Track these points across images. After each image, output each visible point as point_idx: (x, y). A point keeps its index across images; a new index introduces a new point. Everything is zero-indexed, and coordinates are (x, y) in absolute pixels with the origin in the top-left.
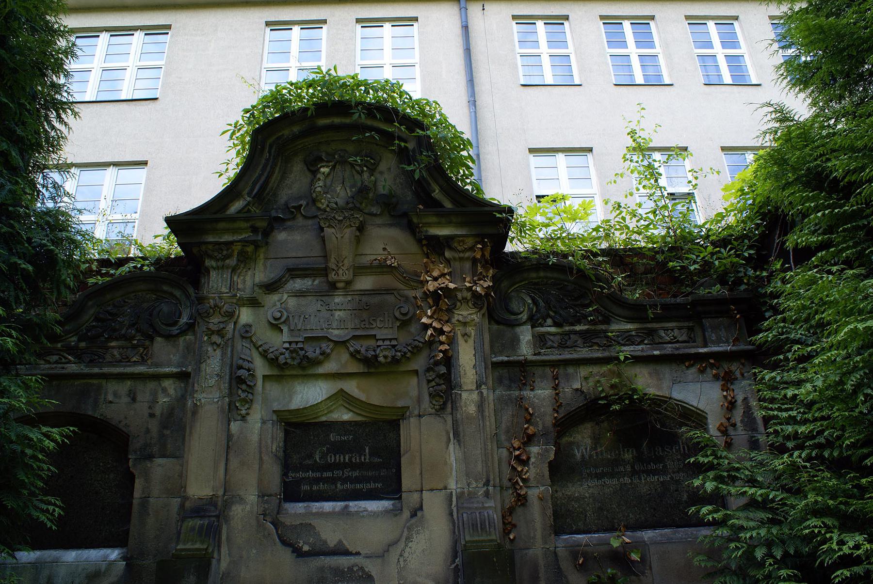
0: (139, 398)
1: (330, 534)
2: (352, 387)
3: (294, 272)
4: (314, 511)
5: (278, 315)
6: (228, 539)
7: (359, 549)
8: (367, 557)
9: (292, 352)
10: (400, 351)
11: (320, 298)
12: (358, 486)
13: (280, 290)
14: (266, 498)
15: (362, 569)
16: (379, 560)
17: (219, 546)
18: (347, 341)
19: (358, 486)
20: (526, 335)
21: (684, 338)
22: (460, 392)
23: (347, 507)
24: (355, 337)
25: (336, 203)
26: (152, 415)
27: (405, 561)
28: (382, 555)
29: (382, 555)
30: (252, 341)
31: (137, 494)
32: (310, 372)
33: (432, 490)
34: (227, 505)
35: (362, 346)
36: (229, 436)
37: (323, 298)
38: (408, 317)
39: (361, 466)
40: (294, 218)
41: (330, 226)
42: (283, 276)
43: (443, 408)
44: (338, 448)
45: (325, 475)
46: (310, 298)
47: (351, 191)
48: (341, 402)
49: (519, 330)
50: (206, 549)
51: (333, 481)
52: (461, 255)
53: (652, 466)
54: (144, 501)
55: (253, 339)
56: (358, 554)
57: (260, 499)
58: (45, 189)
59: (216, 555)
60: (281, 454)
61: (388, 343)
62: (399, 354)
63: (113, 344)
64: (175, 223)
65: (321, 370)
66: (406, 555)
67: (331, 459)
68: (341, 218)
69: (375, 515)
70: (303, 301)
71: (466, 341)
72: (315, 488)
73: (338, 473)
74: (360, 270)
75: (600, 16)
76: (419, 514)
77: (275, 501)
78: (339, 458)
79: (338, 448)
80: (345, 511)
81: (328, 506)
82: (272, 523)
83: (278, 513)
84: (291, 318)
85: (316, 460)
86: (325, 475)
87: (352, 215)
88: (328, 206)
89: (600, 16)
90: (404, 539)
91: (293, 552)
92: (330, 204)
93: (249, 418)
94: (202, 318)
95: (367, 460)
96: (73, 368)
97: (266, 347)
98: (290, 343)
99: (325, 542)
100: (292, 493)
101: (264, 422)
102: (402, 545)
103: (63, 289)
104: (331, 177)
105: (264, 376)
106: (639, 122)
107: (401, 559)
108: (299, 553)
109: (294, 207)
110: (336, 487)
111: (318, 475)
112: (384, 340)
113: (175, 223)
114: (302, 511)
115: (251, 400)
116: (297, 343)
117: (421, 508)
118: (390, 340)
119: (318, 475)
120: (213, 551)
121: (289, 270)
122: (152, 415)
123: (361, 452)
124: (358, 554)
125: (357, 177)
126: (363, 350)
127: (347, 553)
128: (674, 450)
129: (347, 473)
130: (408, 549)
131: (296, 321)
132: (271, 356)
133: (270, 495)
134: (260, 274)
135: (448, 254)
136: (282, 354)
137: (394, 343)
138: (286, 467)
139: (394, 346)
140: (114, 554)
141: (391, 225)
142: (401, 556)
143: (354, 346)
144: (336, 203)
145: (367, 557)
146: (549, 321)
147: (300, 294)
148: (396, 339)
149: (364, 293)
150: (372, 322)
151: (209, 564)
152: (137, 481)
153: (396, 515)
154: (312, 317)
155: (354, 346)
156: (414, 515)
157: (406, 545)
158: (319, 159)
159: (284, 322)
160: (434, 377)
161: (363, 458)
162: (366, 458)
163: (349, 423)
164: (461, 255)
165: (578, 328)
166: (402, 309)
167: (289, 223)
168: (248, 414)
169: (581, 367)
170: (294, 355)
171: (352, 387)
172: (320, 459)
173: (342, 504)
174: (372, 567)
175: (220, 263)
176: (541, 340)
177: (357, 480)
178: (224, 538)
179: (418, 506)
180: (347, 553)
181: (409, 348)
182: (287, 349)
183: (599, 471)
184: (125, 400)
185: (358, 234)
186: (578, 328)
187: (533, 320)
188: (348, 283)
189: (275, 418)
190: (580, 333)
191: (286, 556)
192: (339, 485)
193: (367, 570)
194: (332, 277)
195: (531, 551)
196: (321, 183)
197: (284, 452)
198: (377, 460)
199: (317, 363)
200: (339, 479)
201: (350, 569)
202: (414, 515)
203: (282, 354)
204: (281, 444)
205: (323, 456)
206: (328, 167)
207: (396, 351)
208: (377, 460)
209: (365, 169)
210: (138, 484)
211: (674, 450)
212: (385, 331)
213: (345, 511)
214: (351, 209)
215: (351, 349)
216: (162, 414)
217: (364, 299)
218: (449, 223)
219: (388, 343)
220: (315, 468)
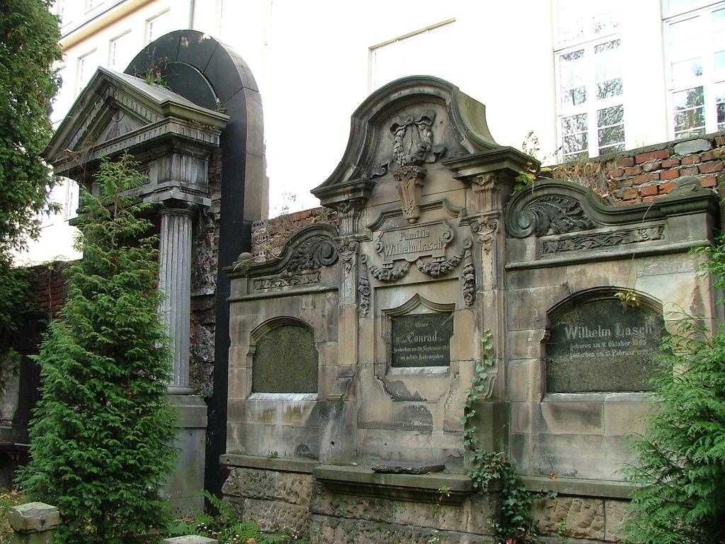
0: (317, 306)
1: (412, 388)
15: (425, 409)
16: (435, 405)
18: (416, 261)
19: (430, 357)
20: (531, 244)
21: (656, 235)
23: (422, 371)
24: (421, 258)
26: (323, 316)
32: (398, 284)
38: (451, 238)
39: (433, 344)
44: (420, 332)
49: (526, 240)
51: (417, 353)
52: (483, 188)
53: (622, 344)
56: (426, 400)
62: (443, 268)
63: (304, 272)
64: (317, 193)
67: (416, 339)
69: (435, 376)
71: (487, 254)
72: (408, 358)
75: (312, 192)
79: (420, 332)
80: (421, 375)
81: (413, 370)
89: (312, 192)
96: (286, 290)
100: (395, 361)
105: (376, 288)
106: (578, 76)
108: (396, 399)
113: (318, 193)
114: (398, 373)
121: (383, 214)
122: (323, 316)
123: (432, 334)
127: (420, 400)
128: (640, 331)
130: (450, 399)
131: (388, 249)
134: (368, 218)
141: (443, 169)
146: (551, 231)
153: (446, 376)
155: (420, 263)
162: (435, 339)
164: (483, 188)
165: (572, 234)
169: (568, 267)
173: (421, 368)
174: (431, 408)
175: (346, 215)
176: (543, 249)
177: (430, 353)
180: (420, 400)
183: (582, 347)
184: (311, 307)
186: (572, 234)
187: (539, 232)
189: (384, 314)
190: (572, 238)
191: (387, 400)
195: (525, 403)
199: (399, 277)
211: (640, 331)
212: (438, 251)
213: (421, 375)
218: (470, 167)
220: (408, 346)
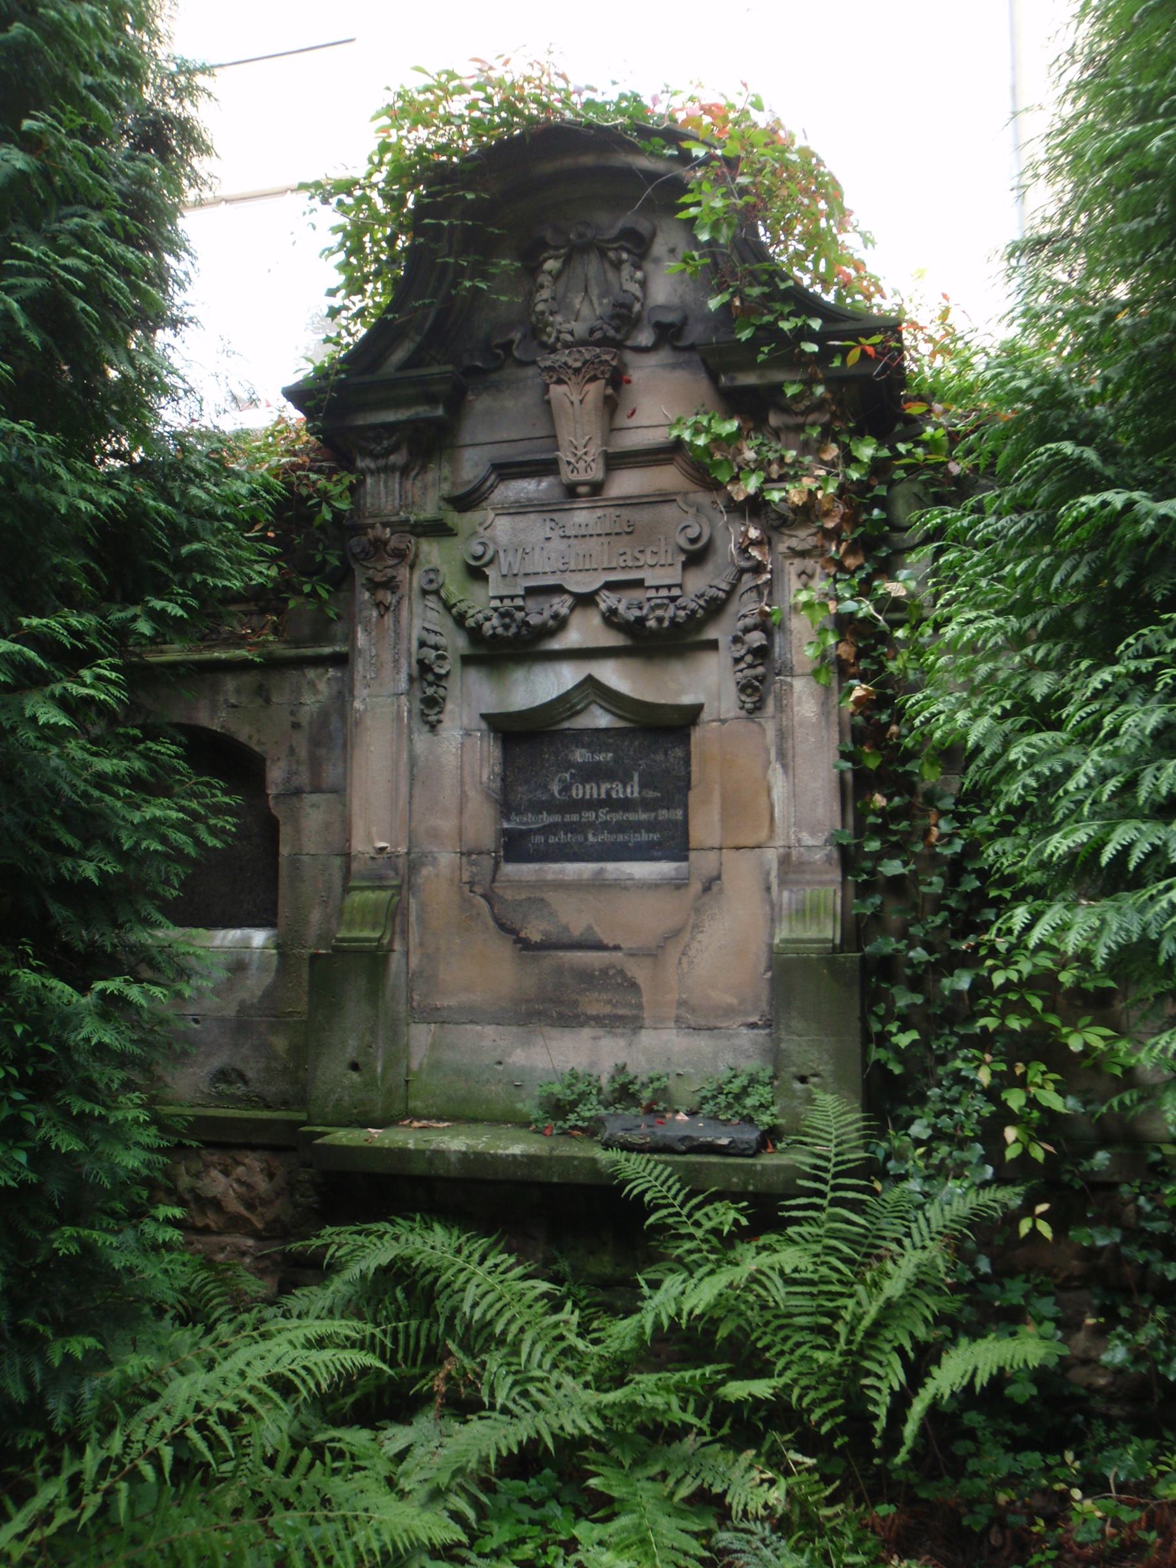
2: (612, 675)
3: (506, 470)
4: (550, 877)
5: (479, 550)
6: (421, 921)
7: (618, 942)
8: (632, 954)
9: (503, 615)
10: (684, 608)
11: (548, 516)
12: (621, 838)
13: (484, 504)
14: (474, 857)
15: (621, 972)
17: (405, 933)
19: (621, 838)
22: (789, 679)
24: (610, 586)
25: (571, 333)
27: (691, 963)
28: (653, 954)
29: (653, 954)
30: (440, 598)
31: (284, 850)
33: (738, 848)
34: (414, 867)
35: (623, 604)
36: (413, 762)
37: (555, 516)
40: (499, 368)
41: (560, 382)
42: (485, 479)
43: (759, 707)
45: (567, 818)
46: (532, 516)
47: (601, 304)
48: (592, 697)
50: (381, 938)
54: (295, 860)
55: (443, 594)
56: (617, 948)
57: (464, 859)
58: (1072, 806)
59: (397, 946)
60: (497, 784)
61: (664, 593)
62: (682, 613)
65: (556, 645)
66: (692, 953)
67: (577, 792)
68: (578, 364)
70: (522, 522)
73: (589, 816)
74: (616, 461)
76: (715, 888)
77: (487, 862)
78: (591, 791)
82: (484, 896)
83: (493, 880)
84: (501, 554)
85: (553, 795)
86: (567, 818)
87: (598, 356)
88: (558, 339)
90: (689, 928)
91: (515, 942)
92: (562, 336)
93: (440, 726)
94: (357, 560)
95: (636, 795)
97: (462, 607)
98: (501, 598)
99: (566, 928)
101: (467, 733)
102: (686, 937)
103: (612, 639)
104: (563, 279)
107: (685, 960)
108: (525, 945)
109: (499, 346)
110: (586, 839)
111: (557, 818)
112: (657, 588)
115: (444, 699)
116: (512, 598)
117: (719, 878)
118: (669, 587)
119: (557, 818)
120: (391, 942)
122: (296, 726)
124: (617, 948)
125: (611, 275)
126: (621, 608)
127: (600, 947)
129: (603, 815)
130: (695, 945)
131: (510, 558)
132: (470, 622)
133: (480, 853)
135: (774, 420)
136: (488, 619)
137: (676, 592)
138: (506, 806)
139: (673, 599)
140: (259, 937)
142: (684, 954)
143: (608, 600)
144: (571, 333)
145: (632, 954)
147: (520, 509)
148: (680, 586)
149: (626, 503)
150: (638, 555)
151: (385, 959)
152: (282, 828)
154: (537, 550)
155: (608, 600)
156: (707, 889)
157: (693, 938)
158: (542, 245)
159: (491, 562)
160: (743, 652)
161: (629, 790)
162: (633, 791)
163: (606, 730)
166: (689, 530)
167: (495, 376)
168: (439, 722)
170: (507, 620)
171: (612, 675)
172: (560, 792)
175: (381, 462)
177: (621, 827)
178: (413, 918)
179: (715, 873)
180: (600, 947)
181: (702, 602)
182: (495, 609)
185: (610, 391)
188: (597, 488)
191: (502, 951)
192: (590, 837)
193: (629, 974)
194: (568, 475)
196: (545, 294)
197: (503, 780)
198: (651, 794)
200: (591, 825)
201: (604, 972)
202: (707, 889)
203: (488, 619)
204: (497, 769)
205: (566, 789)
206: (556, 258)
207: (678, 608)
208: (651, 794)
209: (625, 256)
210: (285, 832)
214: (598, 344)
215: (603, 606)
216: (311, 723)
217: (626, 513)
219: (664, 593)
220: (551, 806)
